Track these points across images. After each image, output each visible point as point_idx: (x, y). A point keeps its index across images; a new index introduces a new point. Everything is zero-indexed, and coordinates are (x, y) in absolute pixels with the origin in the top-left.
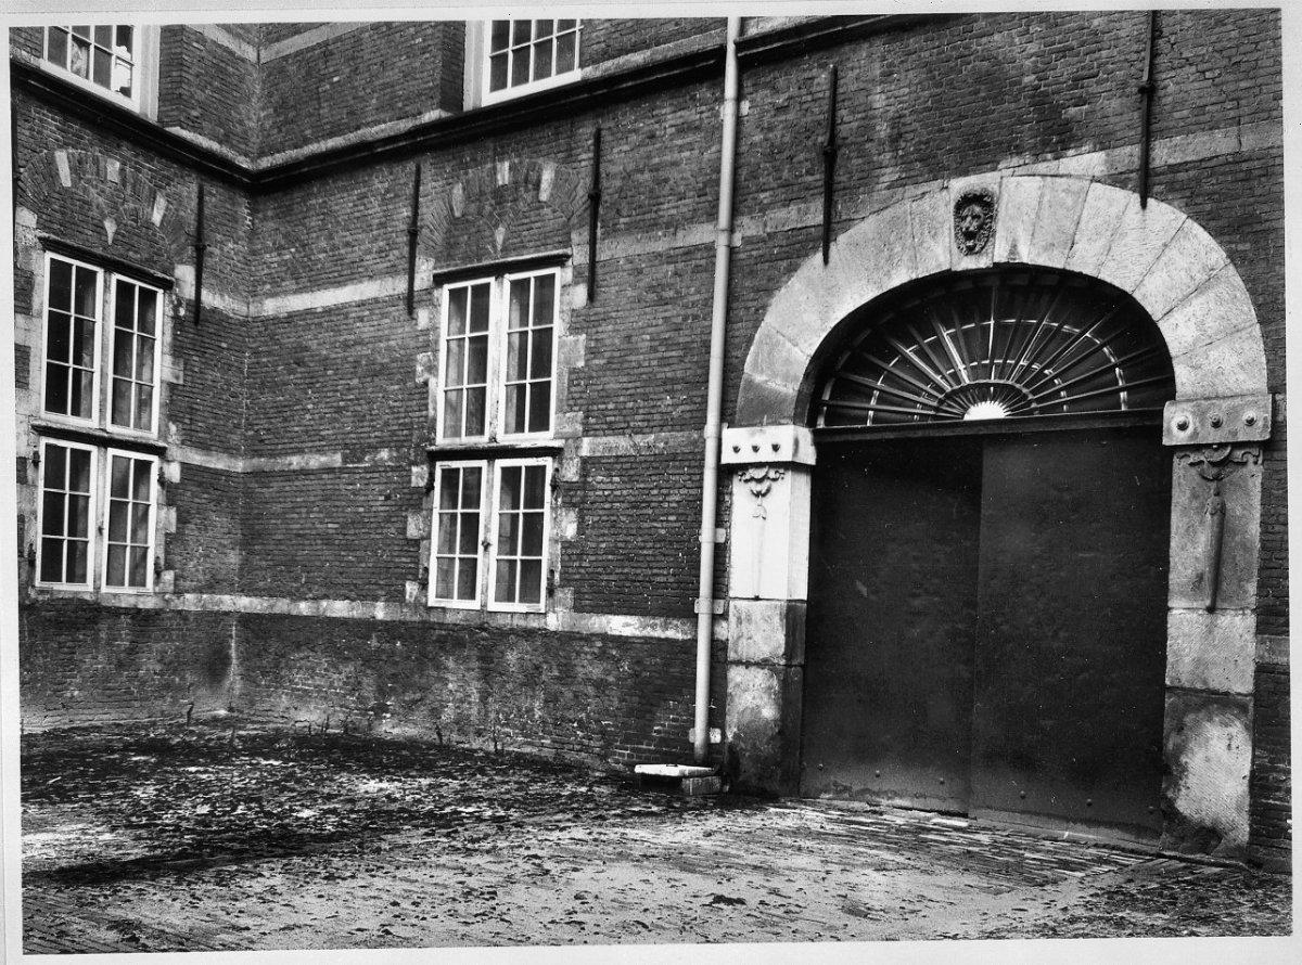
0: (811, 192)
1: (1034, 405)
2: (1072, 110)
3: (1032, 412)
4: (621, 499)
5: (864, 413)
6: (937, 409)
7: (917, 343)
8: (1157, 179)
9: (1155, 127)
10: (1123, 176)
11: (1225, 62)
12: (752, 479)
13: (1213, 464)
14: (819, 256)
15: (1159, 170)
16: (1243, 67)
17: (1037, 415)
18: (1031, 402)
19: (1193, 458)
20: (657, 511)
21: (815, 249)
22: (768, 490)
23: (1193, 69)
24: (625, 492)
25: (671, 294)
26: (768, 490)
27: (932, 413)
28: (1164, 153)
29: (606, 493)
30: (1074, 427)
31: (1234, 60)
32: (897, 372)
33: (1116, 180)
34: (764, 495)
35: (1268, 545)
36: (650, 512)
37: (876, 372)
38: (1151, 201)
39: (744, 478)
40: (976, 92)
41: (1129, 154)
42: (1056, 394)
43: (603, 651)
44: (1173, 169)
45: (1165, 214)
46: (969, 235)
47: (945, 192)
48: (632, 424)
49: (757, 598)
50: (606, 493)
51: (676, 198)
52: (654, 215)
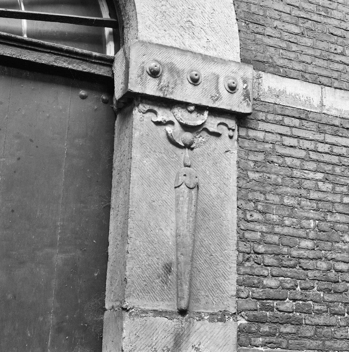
13: (186, 128)
19: (163, 115)
35: (247, 235)
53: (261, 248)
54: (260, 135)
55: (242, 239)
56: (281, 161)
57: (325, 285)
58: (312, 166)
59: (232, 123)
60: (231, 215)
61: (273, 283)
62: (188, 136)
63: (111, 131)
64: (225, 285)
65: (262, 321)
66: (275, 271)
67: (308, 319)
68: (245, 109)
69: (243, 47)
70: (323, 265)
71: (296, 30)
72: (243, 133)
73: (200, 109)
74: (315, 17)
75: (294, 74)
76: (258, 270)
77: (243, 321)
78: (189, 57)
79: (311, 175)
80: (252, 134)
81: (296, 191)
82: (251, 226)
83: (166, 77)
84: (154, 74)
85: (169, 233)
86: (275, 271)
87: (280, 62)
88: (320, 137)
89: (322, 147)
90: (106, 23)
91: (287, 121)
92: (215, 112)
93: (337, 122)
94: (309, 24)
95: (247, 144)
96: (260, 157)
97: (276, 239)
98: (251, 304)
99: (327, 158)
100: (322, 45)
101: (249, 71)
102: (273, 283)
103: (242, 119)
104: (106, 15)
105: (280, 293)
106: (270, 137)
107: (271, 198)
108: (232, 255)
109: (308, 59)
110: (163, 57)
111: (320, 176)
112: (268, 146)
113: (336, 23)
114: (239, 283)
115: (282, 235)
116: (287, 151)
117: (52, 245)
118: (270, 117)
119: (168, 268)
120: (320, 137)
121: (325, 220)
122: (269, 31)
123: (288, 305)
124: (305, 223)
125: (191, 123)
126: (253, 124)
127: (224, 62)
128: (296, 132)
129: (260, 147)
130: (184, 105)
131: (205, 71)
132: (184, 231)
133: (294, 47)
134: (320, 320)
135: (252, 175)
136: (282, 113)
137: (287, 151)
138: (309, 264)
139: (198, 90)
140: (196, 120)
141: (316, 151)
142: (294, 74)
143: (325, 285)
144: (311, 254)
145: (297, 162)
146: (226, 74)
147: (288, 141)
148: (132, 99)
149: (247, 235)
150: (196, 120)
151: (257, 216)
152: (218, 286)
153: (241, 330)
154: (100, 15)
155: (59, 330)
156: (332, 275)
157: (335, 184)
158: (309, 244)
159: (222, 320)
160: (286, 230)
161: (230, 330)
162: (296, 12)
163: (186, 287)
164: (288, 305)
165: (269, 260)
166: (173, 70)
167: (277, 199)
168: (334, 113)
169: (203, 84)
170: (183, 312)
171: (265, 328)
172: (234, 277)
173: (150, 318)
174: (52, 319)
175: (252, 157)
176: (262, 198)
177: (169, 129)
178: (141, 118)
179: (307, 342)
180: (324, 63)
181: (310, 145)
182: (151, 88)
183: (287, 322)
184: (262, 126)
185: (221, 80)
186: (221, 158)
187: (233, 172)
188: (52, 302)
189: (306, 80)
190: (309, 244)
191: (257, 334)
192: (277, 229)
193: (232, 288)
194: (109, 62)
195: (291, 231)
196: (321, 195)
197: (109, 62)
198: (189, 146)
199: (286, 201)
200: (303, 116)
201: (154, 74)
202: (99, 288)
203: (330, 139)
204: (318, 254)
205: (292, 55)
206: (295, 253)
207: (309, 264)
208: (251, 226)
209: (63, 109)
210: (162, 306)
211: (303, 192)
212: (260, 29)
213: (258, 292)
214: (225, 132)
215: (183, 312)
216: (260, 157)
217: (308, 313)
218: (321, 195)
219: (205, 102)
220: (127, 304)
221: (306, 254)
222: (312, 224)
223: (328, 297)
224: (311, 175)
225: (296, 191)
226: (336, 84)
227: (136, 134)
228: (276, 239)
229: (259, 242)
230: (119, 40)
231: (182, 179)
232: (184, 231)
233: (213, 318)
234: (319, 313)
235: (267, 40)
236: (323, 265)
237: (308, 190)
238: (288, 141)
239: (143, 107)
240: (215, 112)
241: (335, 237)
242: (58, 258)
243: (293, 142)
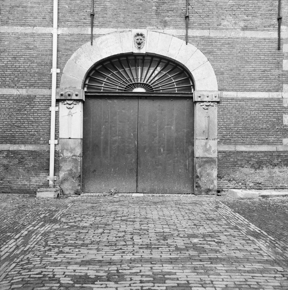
0: (86, 25)
1: (154, 89)
2: (167, 18)
3: (153, 91)
4: (14, 108)
5: (102, 82)
6: (125, 88)
7: (124, 68)
8: (189, 39)
9: (189, 26)
10: (181, 36)
11: (205, 15)
12: (67, 104)
13: (206, 106)
14: (89, 43)
15: (190, 37)
16: (210, 17)
17: (155, 92)
18: (153, 89)
19: (202, 104)
20: (29, 112)
21: (87, 41)
22: (73, 107)
23: (198, 15)
24: (15, 106)
25: (32, 47)
26: (73, 107)
27: (124, 89)
28: (191, 33)
29: (7, 106)
30: (177, 96)
31: (208, 15)
32: (121, 72)
33: (180, 37)
34: (71, 109)
35: (219, 124)
36: (26, 112)
37: (109, 72)
38: (188, 43)
39: (64, 103)
40: (139, 8)
41: (183, 32)
42: (174, 85)
43: (7, 156)
44: (194, 37)
45: (191, 47)
46: (139, 44)
47: (130, 32)
48: (17, 85)
49: (70, 138)
50: (7, 106)
51: (33, 18)
52: (24, 22)
53: (222, 127)
54: (222, 104)
55: (218, 125)
56: (227, 109)
57: (237, 132)
58: (234, 109)
59: (216, 103)
60: (216, 121)
61: (225, 133)
62: (207, 107)
63: (194, 106)
64: (215, 133)
65: (223, 140)
66: (225, 131)
67: (232, 139)
68: (218, 100)
69: (219, 87)
70: (236, 129)
71: (231, 80)
72: (219, 105)
73: (209, 102)
74: (236, 76)
75: (230, 90)
76: (222, 131)
77: (219, 140)
78: (206, 92)
79: (234, 111)
80: (220, 104)
81: (230, 115)
82: (220, 123)
83: (202, 97)
84: (200, 97)
85: (204, 125)
86: (225, 131)
87: (227, 88)
88: (236, 103)
89: (236, 105)
90: (192, 86)
91: (229, 101)
92: (212, 102)
93: (240, 99)
94: (234, 78)
95: (219, 107)
96: (222, 109)
97: (226, 124)
98: (220, 137)
99: (238, 107)
100: (237, 82)
101: (219, 92)
102: (225, 133)
103: (218, 102)
104: (191, 84)
105: (227, 135)
106: (225, 105)
107: (225, 117)
108: (217, 128)
109: (234, 86)
110: (201, 93)
111: (236, 111)
112: (224, 107)
113: (241, 76)
114: (218, 133)
115: (227, 124)
116: (229, 107)
117: (184, 128)
118: (225, 100)
119: (204, 132)
120: (236, 103)
121: (237, 120)
122: (225, 82)
123: (228, 137)
124: (232, 121)
125: (207, 105)
126: (221, 103)
127: (214, 91)
128: (231, 103)
129: (222, 107)
130: (206, 102)
131: (210, 94)
132: (206, 125)
133: (231, 84)
134: (235, 139)
135: (220, 113)
136: (227, 99)
137: (229, 107)
138: (233, 129)
139: (209, 98)
140: (208, 104)
141: (235, 106)
142: (230, 90)
143: (237, 132)
144: (233, 127)
145: (231, 109)
146: (214, 94)
147: (229, 105)
148: (196, 102)
149: (219, 124)
150: (208, 104)
151: (221, 121)
152: (214, 134)
153: (218, 142)
154: (190, 84)
155: (186, 142)
156: (238, 130)
157: (239, 112)
158: (233, 125)
159: (214, 140)
160: (228, 123)
161: (216, 141)
162: (231, 76)
163: (207, 135)
164: (228, 137)
165: (224, 129)
166: (203, 95)
167: (226, 117)
168: (240, 97)
169: (210, 97)
170: (207, 139)
171: (223, 141)
172: (217, 132)
173: (201, 140)
174: (185, 141)
175: (220, 109)
176: (222, 117)
177: (203, 106)
178: (198, 105)
179: (232, 143)
180: (238, 86)
181: (234, 105)
182: (199, 100)
183: (228, 140)
184: (223, 103)
185: (213, 95)
186: (214, 110)
187: (216, 113)
188: (185, 138)
189: (233, 91)
190: (233, 125)
191: (221, 142)
192: (226, 123)
193: (216, 134)
194: (192, 94)
195: (229, 123)
196: (236, 115)
197: (192, 94)
198: (207, 109)
199: (228, 117)
200: (232, 99)
201: (200, 97)
202: (193, 135)
203: (239, 103)
204: (235, 127)
205: (230, 86)
206: (230, 127)
207: (233, 129)
208: (220, 123)
209: (186, 103)
210: (203, 138)
211: (232, 115)
212: (223, 82)
213: (222, 135)
214: (215, 105)
215: (207, 139)
216: (222, 109)
217: (233, 138)
218: (236, 115)
219: (210, 100)
220: (197, 138)
221: (232, 127)
222: (234, 121)
223: (237, 135)
224: (234, 111)
225: (230, 115)
226: (241, 90)
227: (197, 108)
228: (226, 124)
229: (222, 125)
230: (194, 90)
231: (206, 116)
232: (206, 125)
233: (213, 139)
234: (235, 138)
235: (224, 84)
236: (236, 129)
237: (233, 114)
238: (229, 105)
239: (198, 103)
240: (212, 102)
241: (239, 123)
242: (185, 130)
243: (230, 105)
